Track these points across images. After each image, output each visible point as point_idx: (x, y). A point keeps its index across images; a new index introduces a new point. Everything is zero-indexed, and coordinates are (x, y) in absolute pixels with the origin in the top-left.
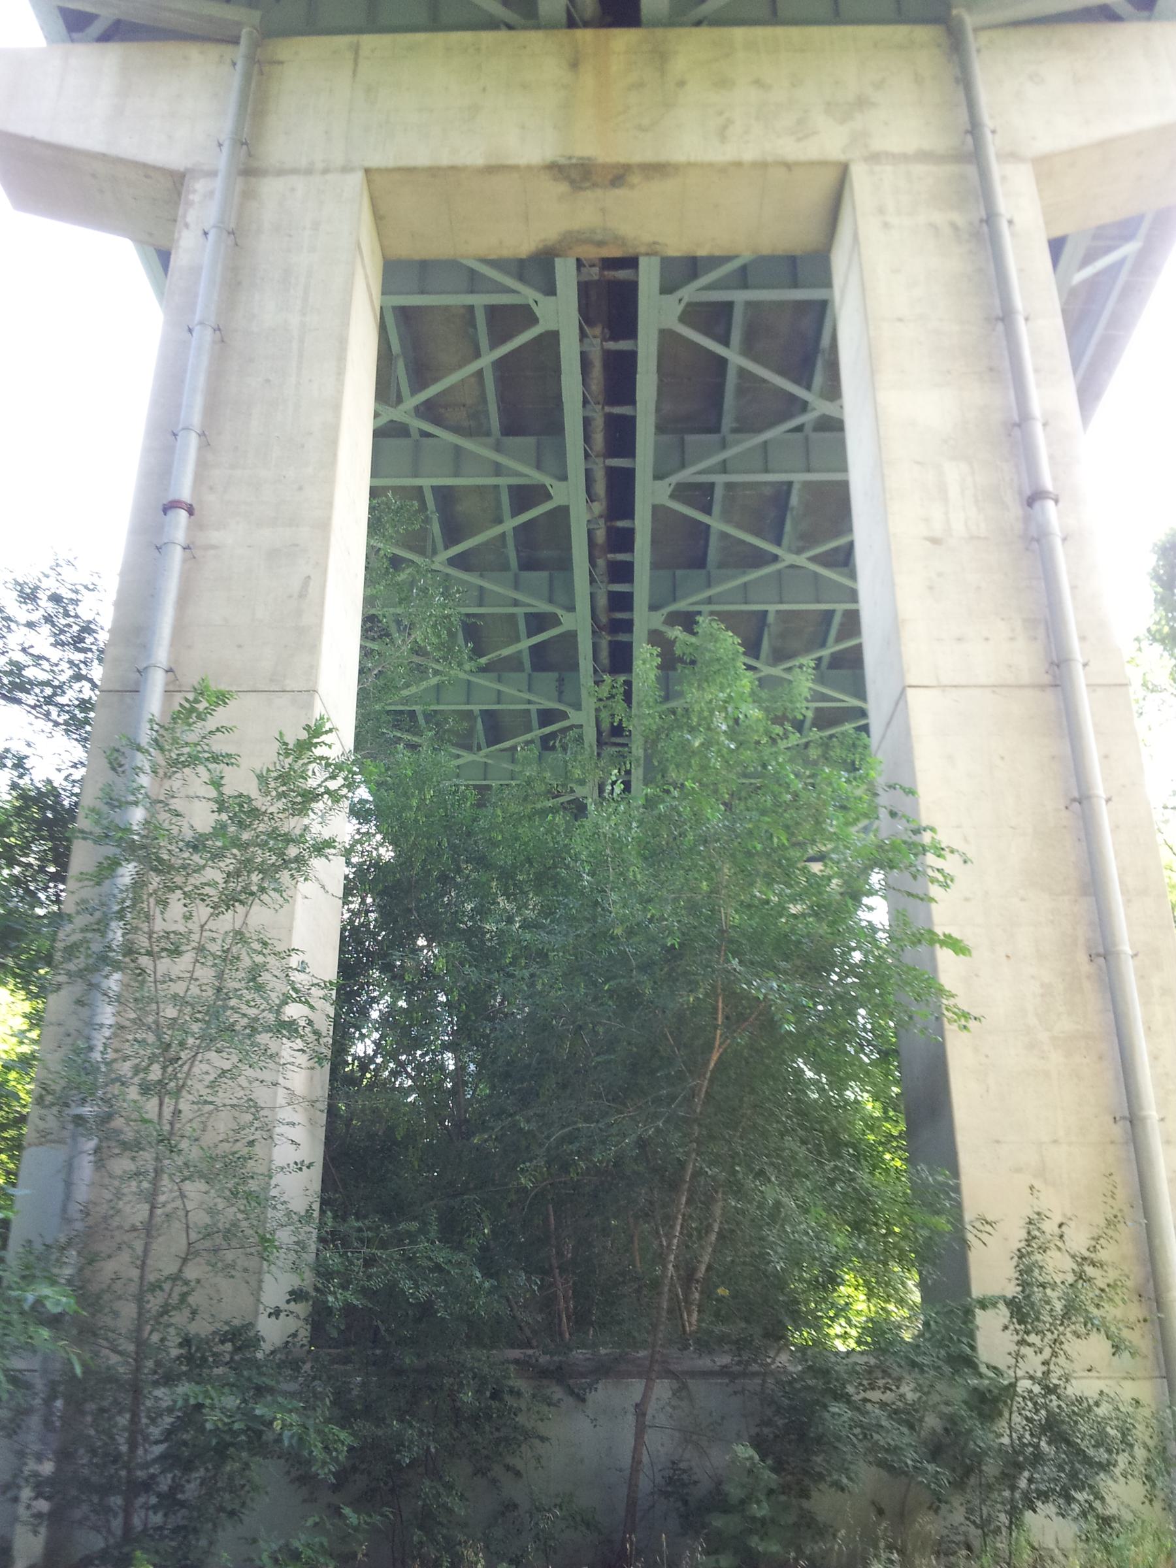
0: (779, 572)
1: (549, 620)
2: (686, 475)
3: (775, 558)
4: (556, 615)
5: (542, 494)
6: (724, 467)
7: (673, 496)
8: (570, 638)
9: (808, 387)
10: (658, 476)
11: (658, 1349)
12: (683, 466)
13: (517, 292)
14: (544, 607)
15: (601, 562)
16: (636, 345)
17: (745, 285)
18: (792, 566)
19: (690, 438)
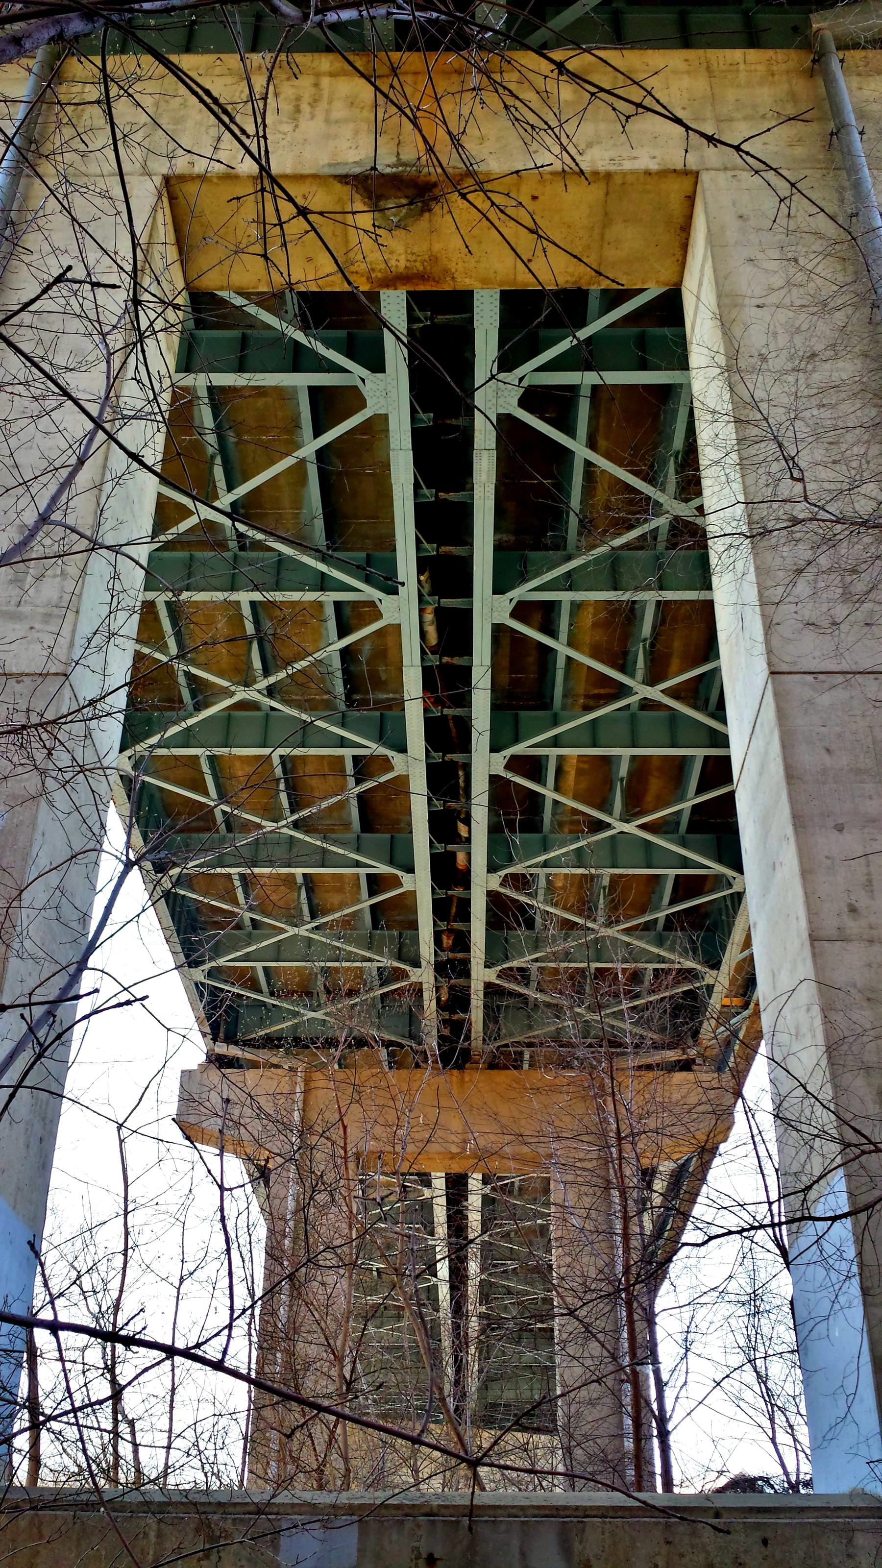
0: (612, 837)
1: (399, 975)
2: (519, 749)
3: (608, 826)
4: (396, 876)
5: (371, 611)
6: (545, 864)
7: (514, 615)
8: (401, 785)
9: (610, 814)
10: (495, 748)
11: (25, 732)
12: (516, 740)
13: (347, 371)
14: (383, 869)
15: (430, 609)
16: (472, 603)
17: (556, 746)
18: (622, 832)
19: (523, 714)
